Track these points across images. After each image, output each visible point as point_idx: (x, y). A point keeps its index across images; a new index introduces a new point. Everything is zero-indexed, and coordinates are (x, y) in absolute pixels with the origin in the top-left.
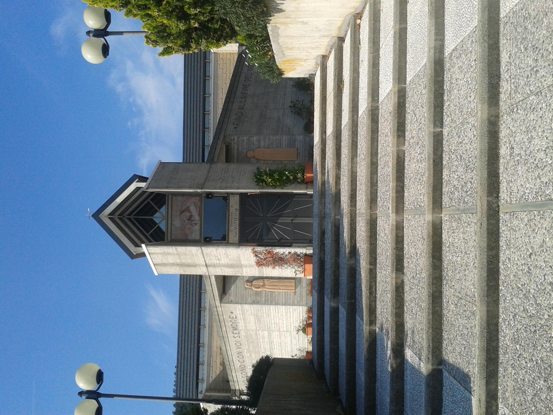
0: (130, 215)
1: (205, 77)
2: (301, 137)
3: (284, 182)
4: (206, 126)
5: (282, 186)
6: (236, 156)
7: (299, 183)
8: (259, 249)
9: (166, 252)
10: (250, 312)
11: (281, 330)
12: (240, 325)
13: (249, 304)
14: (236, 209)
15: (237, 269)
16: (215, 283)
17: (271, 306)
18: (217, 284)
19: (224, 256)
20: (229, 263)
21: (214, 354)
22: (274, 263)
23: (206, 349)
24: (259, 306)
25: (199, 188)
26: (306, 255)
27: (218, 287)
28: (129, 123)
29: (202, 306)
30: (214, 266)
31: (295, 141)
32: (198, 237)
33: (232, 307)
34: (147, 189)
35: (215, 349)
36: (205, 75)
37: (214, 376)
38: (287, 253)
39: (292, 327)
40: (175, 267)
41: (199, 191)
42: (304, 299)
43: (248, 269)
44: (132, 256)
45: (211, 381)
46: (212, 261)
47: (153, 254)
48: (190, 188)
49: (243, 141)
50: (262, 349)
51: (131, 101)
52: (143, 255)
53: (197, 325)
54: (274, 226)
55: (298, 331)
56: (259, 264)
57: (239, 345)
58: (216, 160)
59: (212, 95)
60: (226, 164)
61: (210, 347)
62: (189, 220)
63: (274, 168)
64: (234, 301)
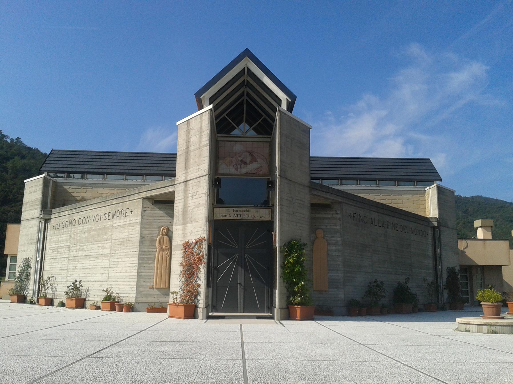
0: (248, 95)
1: (399, 181)
2: (343, 296)
3: (291, 278)
4: (344, 182)
5: (284, 276)
6: (317, 216)
7: (288, 297)
8: (204, 246)
9: (203, 134)
10: (131, 233)
11: (110, 269)
12: (118, 221)
14: (253, 216)
15: (181, 218)
16: (166, 191)
17: (137, 258)
18: (165, 194)
19: (197, 203)
20: (189, 208)
21: (94, 190)
22: (186, 265)
23: (374, 187)
24: (138, 244)
25: (281, 171)
26: (196, 307)
27: (162, 194)
28: (329, 113)
29: (148, 177)
30: (186, 191)
32: (221, 171)
33: (138, 212)
34: (279, 111)
35: (100, 191)
36: (399, 180)
37: (70, 190)
38: (199, 282)
39: (113, 283)
40: (185, 144)
41: (277, 173)
42: (144, 300)
43: (181, 232)
44: (198, 95)
45: (65, 187)
46: (191, 188)
47: (201, 118)
48: (281, 161)
50: (91, 246)
51: (349, 115)
52: (201, 107)
53: (126, 171)
54: (234, 262)
55: (107, 292)
56: (187, 246)
57: (96, 219)
58: (315, 192)
59: (379, 188)
60: (309, 205)
61: (103, 186)
62: (242, 161)
63: (305, 264)
64: (145, 214)
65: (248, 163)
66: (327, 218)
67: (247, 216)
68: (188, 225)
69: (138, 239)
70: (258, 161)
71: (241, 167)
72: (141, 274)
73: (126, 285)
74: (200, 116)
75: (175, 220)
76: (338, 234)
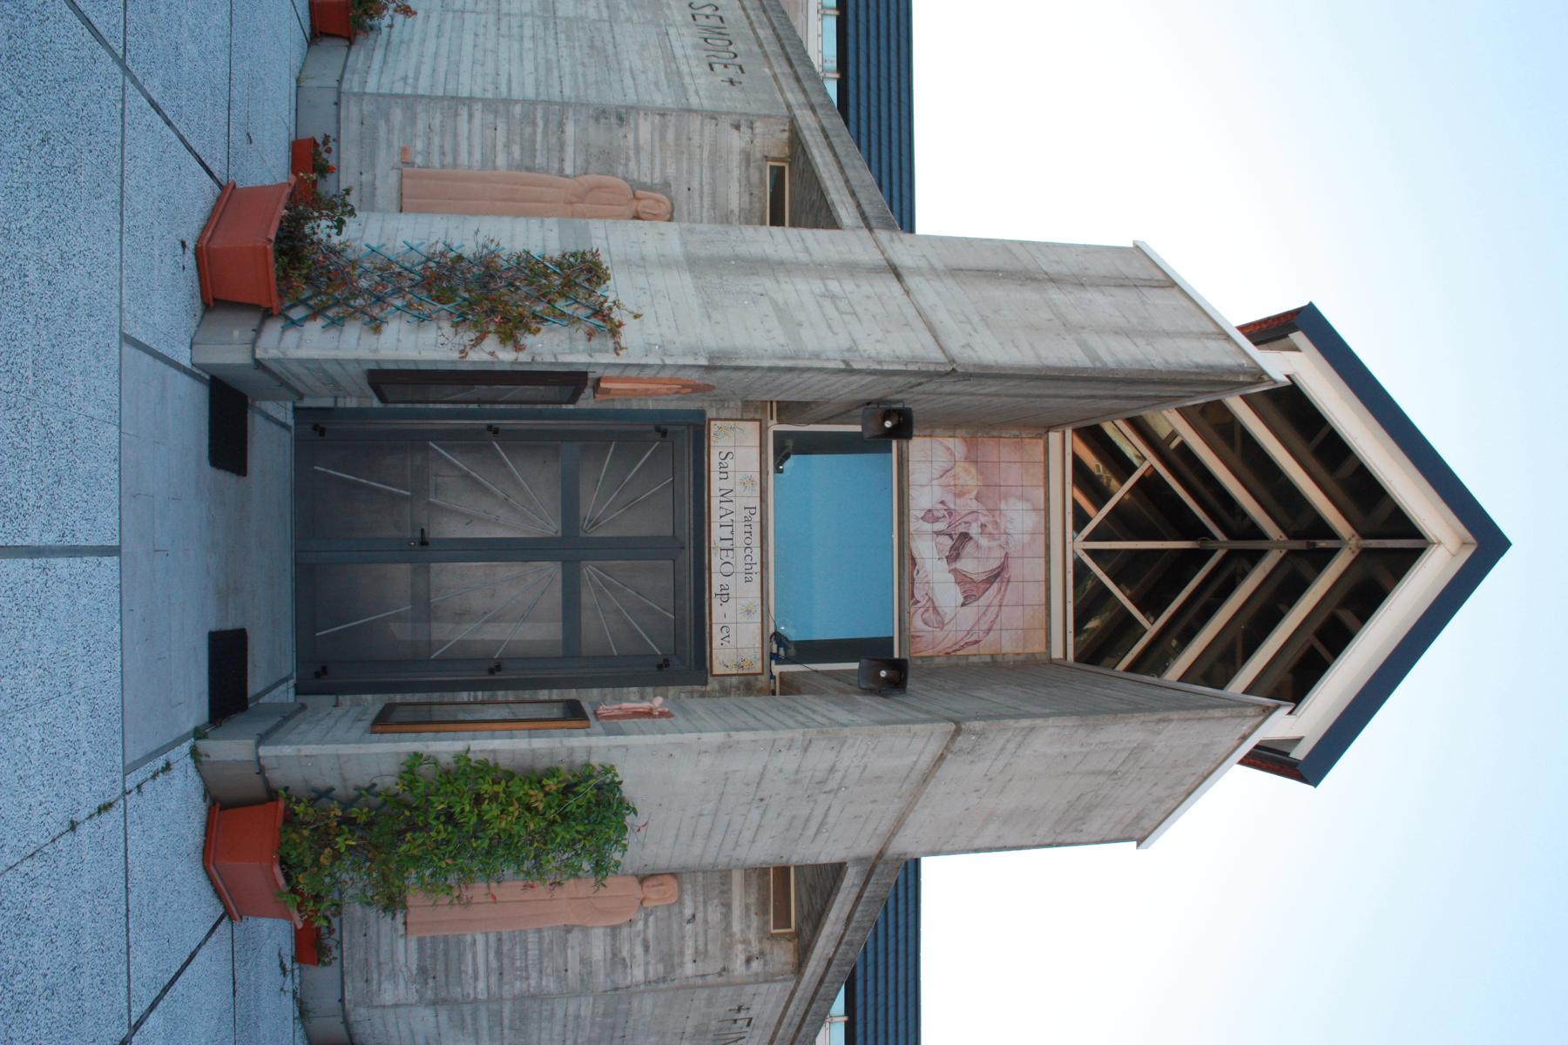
9: (1141, 342)
11: (492, 18)
12: (688, 40)
13: (648, 111)
14: (725, 596)
15: (722, 249)
17: (530, 93)
24: (593, 97)
30: (850, 269)
31: (422, 970)
46: (866, 289)
49: (700, 955)
62: (965, 537)
64: (725, 124)
65: (959, 565)
66: (727, 917)
67: (727, 569)
68: (687, 278)
69: (614, 98)
70: (967, 609)
71: (939, 533)
72: (464, 112)
73: (420, 64)
74: (1211, 328)
75: (704, 227)
76: (661, 968)
